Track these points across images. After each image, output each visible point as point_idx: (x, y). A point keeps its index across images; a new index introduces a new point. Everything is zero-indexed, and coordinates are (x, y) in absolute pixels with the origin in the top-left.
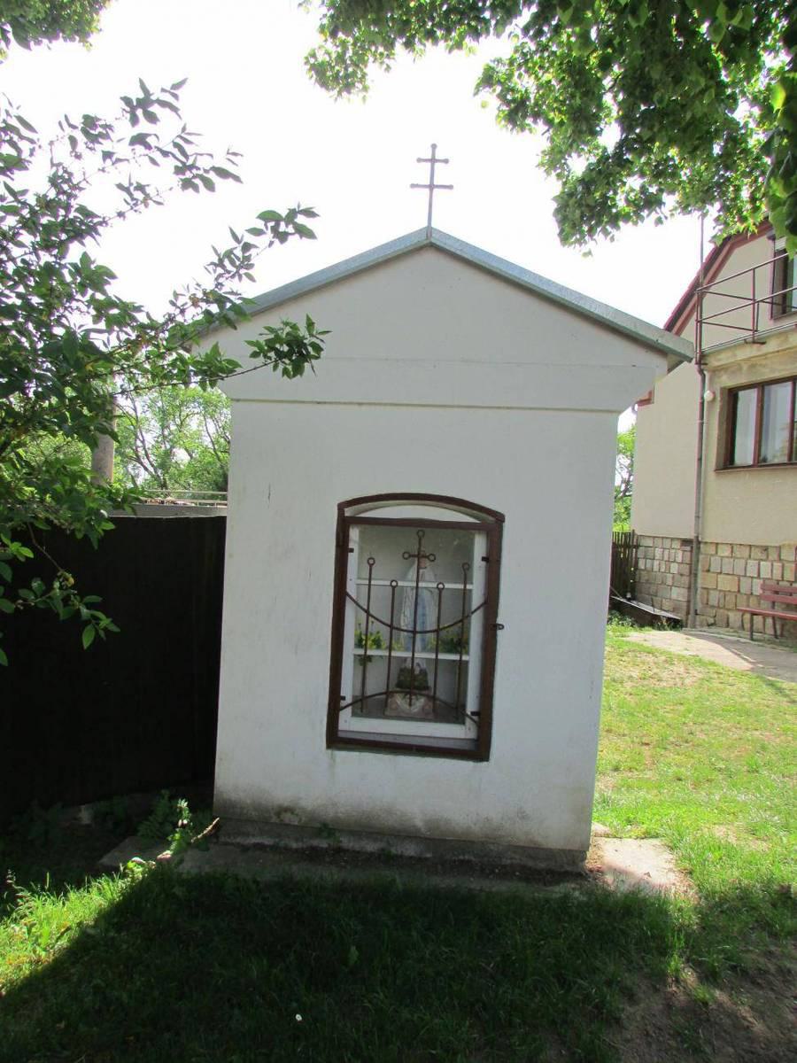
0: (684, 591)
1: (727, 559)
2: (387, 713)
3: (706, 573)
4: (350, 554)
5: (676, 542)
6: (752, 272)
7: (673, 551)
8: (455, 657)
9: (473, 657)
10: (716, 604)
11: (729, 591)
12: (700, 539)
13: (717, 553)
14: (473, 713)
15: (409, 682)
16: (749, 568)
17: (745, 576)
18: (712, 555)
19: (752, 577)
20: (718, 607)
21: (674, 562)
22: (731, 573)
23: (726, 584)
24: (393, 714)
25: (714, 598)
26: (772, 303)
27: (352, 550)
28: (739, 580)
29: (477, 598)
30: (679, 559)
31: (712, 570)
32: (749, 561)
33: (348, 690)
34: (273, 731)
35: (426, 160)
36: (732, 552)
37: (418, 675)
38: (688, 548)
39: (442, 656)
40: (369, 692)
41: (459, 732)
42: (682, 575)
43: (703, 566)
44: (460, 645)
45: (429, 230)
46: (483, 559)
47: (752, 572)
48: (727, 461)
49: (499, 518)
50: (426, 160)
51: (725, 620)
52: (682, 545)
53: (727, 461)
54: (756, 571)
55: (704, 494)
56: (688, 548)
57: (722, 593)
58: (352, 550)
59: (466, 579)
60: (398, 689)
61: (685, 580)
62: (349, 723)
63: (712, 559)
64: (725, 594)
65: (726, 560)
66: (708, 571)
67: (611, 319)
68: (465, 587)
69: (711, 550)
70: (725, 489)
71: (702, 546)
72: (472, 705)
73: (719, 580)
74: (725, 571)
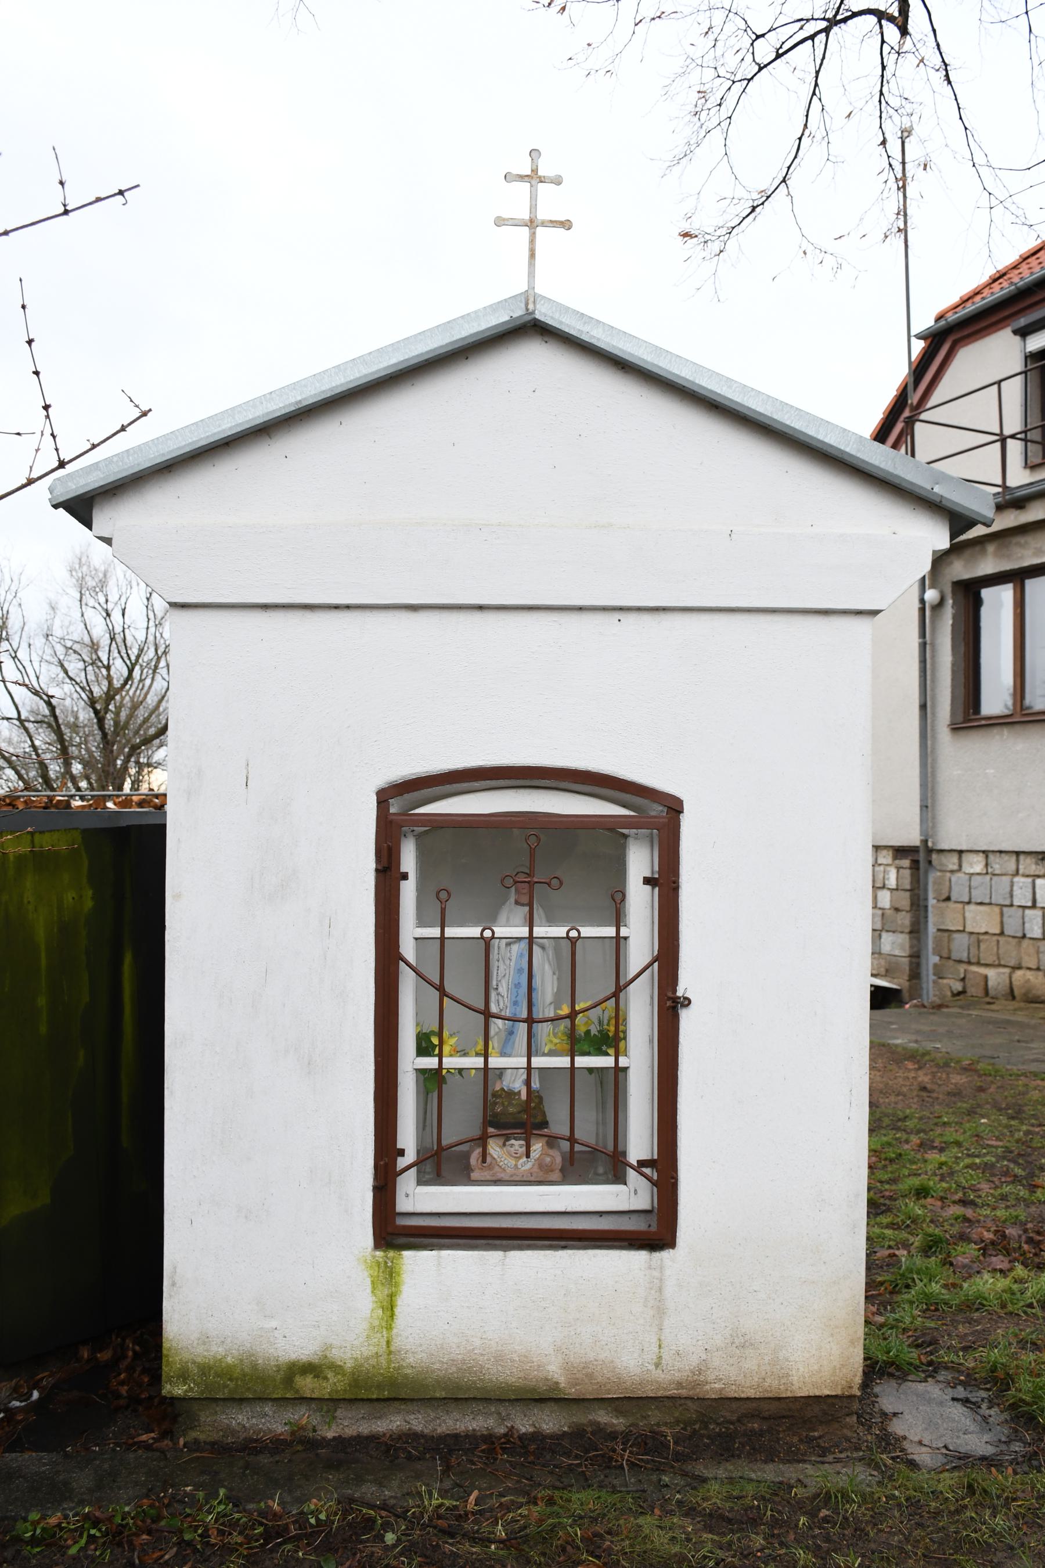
0: (903, 939)
1: (978, 878)
2: (474, 1175)
3: (944, 904)
4: (403, 883)
5: (885, 852)
6: (996, 386)
7: (882, 868)
8: (608, 1062)
9: (639, 1058)
10: (964, 956)
11: (986, 933)
12: (930, 844)
13: (960, 866)
14: (642, 1163)
15: (515, 1117)
16: (1017, 891)
17: (1012, 905)
18: (952, 872)
19: (1024, 907)
20: (969, 963)
21: (884, 887)
22: (987, 901)
23: (980, 920)
24: (487, 1175)
25: (960, 946)
26: (1025, 440)
28: (1002, 914)
30: (892, 882)
31: (953, 898)
32: (1016, 879)
35: (521, 178)
36: (987, 865)
38: (906, 863)
39: (581, 1061)
40: (445, 1142)
42: (897, 910)
43: (938, 891)
44: (611, 1040)
46: (647, 881)
47: (1022, 897)
48: (969, 714)
49: (674, 807)
50: (521, 178)
51: (983, 983)
52: (895, 858)
53: (969, 714)
54: (1030, 896)
55: (933, 767)
56: (906, 863)
57: (974, 937)
58: (647, 881)
59: (618, 919)
61: (905, 920)
62: (418, 1198)
63: (953, 879)
64: (977, 937)
65: (976, 881)
66: (948, 899)
67: (853, 453)
69: (952, 862)
70: (962, 758)
71: (934, 856)
72: (639, 1143)
73: (967, 914)
74: (977, 896)
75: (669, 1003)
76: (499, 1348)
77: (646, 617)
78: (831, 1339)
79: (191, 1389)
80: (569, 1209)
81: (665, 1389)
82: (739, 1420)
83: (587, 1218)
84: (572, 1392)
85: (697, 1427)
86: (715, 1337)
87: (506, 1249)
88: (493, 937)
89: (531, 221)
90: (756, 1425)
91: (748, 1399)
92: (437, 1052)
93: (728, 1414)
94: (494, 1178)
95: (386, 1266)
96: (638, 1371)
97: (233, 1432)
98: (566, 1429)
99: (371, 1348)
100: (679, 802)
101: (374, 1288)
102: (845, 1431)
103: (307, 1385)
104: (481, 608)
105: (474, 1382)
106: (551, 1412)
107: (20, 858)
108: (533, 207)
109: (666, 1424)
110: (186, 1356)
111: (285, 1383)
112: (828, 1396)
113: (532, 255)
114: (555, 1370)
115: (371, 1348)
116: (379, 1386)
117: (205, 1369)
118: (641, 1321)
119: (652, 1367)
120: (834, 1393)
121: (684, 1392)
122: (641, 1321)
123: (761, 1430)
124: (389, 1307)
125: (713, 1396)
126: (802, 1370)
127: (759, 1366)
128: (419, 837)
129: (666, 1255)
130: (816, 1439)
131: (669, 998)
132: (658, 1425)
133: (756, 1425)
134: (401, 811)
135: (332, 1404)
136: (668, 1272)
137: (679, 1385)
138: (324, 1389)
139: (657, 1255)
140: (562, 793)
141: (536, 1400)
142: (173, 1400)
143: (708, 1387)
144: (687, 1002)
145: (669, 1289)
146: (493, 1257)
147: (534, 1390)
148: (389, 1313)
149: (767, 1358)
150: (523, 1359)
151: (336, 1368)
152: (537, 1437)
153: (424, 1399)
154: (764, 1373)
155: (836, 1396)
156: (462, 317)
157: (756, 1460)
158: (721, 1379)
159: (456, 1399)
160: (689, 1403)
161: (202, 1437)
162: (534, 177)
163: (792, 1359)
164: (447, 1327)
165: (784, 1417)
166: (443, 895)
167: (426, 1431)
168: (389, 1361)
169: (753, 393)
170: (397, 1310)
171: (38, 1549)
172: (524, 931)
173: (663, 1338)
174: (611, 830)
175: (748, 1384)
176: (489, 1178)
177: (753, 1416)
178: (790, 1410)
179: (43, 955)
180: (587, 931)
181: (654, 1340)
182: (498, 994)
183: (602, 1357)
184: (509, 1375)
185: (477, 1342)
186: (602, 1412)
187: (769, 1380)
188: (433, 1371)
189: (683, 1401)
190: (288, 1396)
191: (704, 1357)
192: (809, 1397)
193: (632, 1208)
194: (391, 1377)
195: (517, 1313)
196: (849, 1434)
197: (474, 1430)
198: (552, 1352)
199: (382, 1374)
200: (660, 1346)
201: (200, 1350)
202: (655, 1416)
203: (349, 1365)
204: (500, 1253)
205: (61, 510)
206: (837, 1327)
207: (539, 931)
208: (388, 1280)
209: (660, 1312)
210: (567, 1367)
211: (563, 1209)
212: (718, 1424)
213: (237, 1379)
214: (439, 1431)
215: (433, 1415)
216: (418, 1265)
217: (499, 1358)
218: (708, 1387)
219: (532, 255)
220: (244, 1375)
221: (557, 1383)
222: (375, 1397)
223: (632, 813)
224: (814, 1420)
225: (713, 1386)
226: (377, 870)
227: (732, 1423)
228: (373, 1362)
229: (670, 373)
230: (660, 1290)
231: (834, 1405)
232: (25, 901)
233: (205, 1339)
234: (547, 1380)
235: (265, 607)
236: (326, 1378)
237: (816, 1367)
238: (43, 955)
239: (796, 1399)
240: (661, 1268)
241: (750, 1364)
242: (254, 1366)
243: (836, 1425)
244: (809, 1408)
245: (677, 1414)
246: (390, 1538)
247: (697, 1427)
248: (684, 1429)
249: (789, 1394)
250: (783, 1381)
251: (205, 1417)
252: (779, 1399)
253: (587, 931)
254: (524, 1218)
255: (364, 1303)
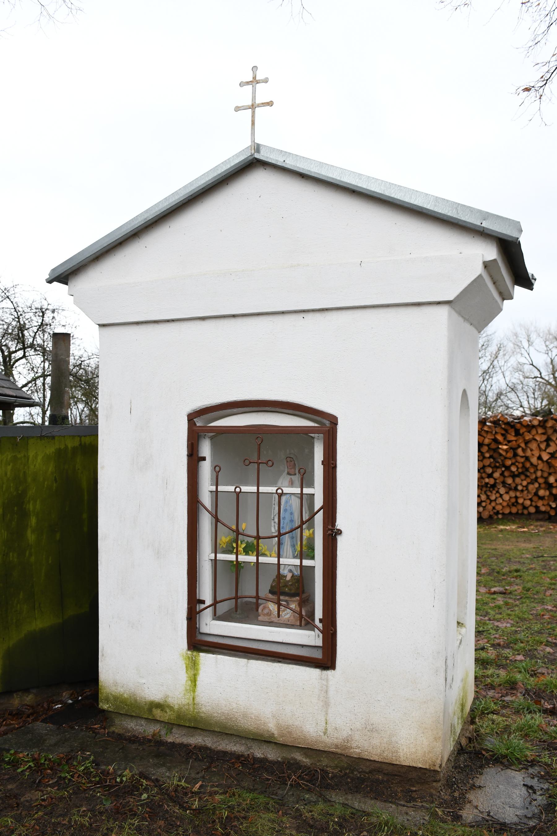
2: (260, 618)
9: (317, 563)
24: (266, 619)
27: (204, 459)
29: (319, 502)
33: (206, 593)
34: (142, 648)
35: (248, 83)
37: (289, 581)
41: (311, 638)
44: (307, 552)
45: (257, 148)
49: (333, 421)
50: (248, 83)
58: (204, 459)
60: (270, 596)
62: (211, 626)
68: (258, 489)
72: (319, 613)
75: (330, 532)
76: (245, 710)
77: (318, 315)
78: (422, 735)
79: (110, 707)
80: (284, 641)
81: (329, 747)
82: (370, 772)
83: (295, 647)
84: (281, 740)
85: (348, 771)
86: (356, 723)
87: (249, 658)
88: (240, 491)
89: (252, 105)
90: (380, 777)
91: (374, 761)
92: (235, 551)
93: (364, 768)
94: (270, 621)
95: (192, 660)
96: (315, 735)
97: (129, 731)
98: (279, 759)
99: (186, 700)
100: (336, 418)
101: (187, 670)
102: (432, 790)
103: (157, 713)
104: (234, 316)
105: (233, 726)
106: (273, 749)
107: (74, 449)
108: (254, 98)
109: (331, 767)
110: (108, 690)
111: (150, 710)
112: (421, 768)
113: (253, 123)
114: (272, 727)
115: (186, 700)
116: (190, 720)
117: (116, 698)
118: (316, 708)
119: (322, 734)
120: (424, 767)
121: (339, 751)
122: (316, 708)
123: (382, 780)
124: (194, 680)
125: (355, 756)
126: (405, 750)
127: (381, 744)
128: (211, 438)
129: (330, 673)
130: (412, 791)
131: (329, 530)
132: (327, 766)
133: (380, 777)
134: (200, 425)
135: (170, 725)
136: (330, 683)
137: (337, 746)
138: (167, 716)
139: (325, 673)
140: (280, 414)
141: (265, 741)
142: (103, 711)
143: (352, 750)
144: (339, 532)
145: (331, 693)
146: (242, 662)
147: (262, 735)
148: (194, 684)
149: (385, 740)
150: (256, 718)
151: (171, 708)
152: (263, 761)
153: (210, 731)
154: (383, 748)
155: (426, 769)
156: (222, 163)
157: (367, 796)
158: (360, 747)
159: (227, 734)
160: (343, 758)
161: (116, 731)
162: (255, 82)
163: (399, 742)
164: (220, 695)
165: (396, 775)
166: (217, 469)
167: (213, 747)
168: (194, 708)
169: (373, 181)
170: (198, 683)
171: (8, 767)
172: (298, 491)
173: (328, 719)
174: (306, 434)
175: (374, 753)
176: (267, 620)
177: (378, 771)
178: (399, 772)
179: (86, 494)
180: (245, 489)
181: (323, 719)
182: (275, 522)
183: (296, 723)
184: (248, 725)
185: (235, 706)
186: (298, 754)
187: (386, 752)
188: (214, 717)
189: (339, 756)
190: (150, 717)
191: (350, 733)
192: (410, 766)
193: (317, 645)
194: (195, 716)
195: (252, 693)
196: (434, 792)
197: (235, 751)
198: (271, 717)
199: (191, 714)
200: (326, 723)
201: (114, 688)
202: (325, 762)
203: (176, 707)
204: (246, 660)
205: (55, 283)
206: (426, 729)
207: (220, 488)
208: (193, 667)
209: (327, 704)
210: (278, 726)
211: (281, 641)
212: (360, 772)
213: (129, 705)
214: (219, 748)
215: (215, 740)
216: (206, 660)
217: (245, 715)
218: (352, 750)
219: (253, 123)
220: (132, 704)
221: (273, 734)
222: (187, 725)
223: (316, 425)
224: (413, 780)
225: (355, 750)
226: (188, 455)
227: (367, 773)
228: (186, 707)
229: (328, 177)
230: (327, 692)
231: (425, 774)
232: (77, 469)
233: (116, 684)
234: (268, 731)
235: (137, 323)
236: (166, 712)
237: (414, 750)
238: (86, 494)
239: (403, 766)
240: (327, 680)
241: (376, 742)
242: (136, 701)
243: (427, 786)
244: (410, 773)
245: (336, 763)
246: (145, 796)
247: (348, 771)
248: (341, 771)
249: (398, 763)
250: (394, 755)
251: (117, 721)
252: (393, 764)
253: (245, 489)
254: (252, 642)
255: (183, 677)
